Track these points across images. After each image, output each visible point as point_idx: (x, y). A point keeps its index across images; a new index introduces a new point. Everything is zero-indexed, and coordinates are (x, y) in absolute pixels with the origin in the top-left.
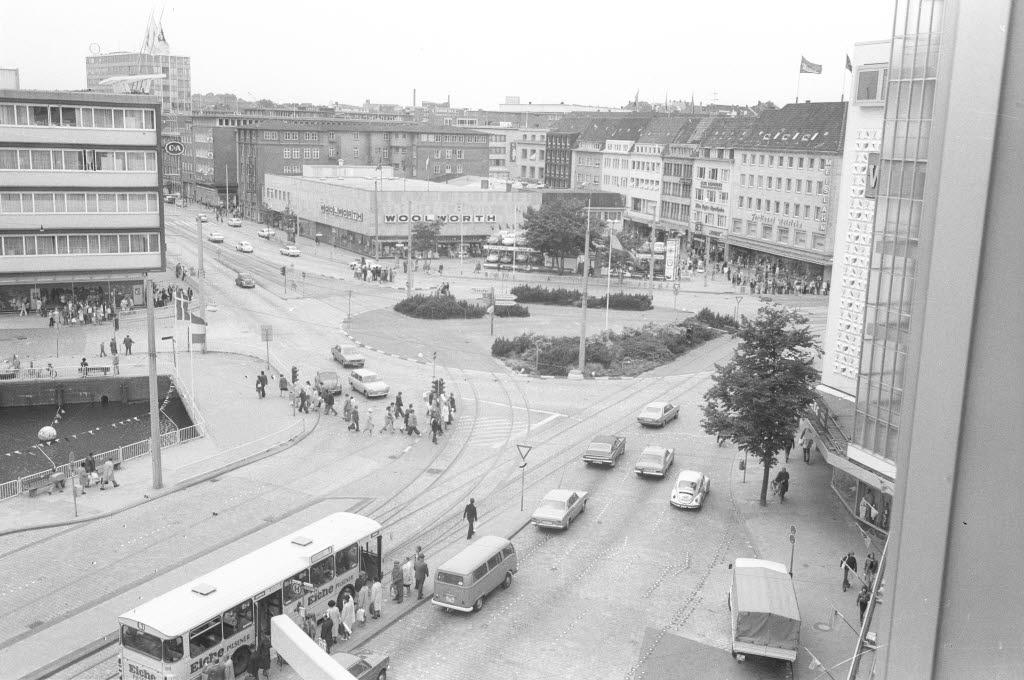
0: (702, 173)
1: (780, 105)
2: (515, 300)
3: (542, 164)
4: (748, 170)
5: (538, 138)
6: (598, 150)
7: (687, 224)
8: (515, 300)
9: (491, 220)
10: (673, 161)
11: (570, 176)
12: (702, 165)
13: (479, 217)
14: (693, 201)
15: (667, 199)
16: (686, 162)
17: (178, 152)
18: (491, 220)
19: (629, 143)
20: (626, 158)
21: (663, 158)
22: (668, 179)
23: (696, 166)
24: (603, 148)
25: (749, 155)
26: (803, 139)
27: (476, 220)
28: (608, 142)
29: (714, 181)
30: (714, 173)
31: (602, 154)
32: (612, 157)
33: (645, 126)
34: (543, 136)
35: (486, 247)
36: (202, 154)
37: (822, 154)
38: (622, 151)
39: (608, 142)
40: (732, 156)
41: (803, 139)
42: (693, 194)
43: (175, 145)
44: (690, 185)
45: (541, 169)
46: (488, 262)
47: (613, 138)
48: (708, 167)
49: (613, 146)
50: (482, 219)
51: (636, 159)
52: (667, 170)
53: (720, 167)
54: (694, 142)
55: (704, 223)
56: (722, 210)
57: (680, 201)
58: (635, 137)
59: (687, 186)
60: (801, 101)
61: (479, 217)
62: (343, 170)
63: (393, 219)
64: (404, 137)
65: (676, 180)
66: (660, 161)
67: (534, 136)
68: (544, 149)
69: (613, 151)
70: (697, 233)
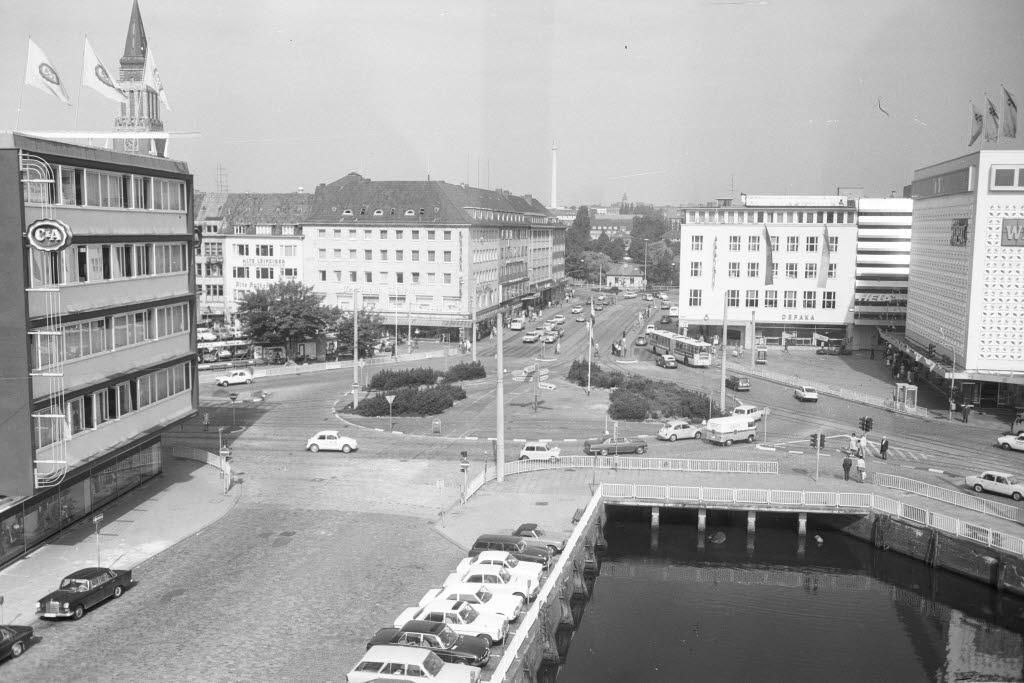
40: (299, 229)
42: (228, 270)
48: (252, 244)
53: (276, 244)
54: (209, 219)
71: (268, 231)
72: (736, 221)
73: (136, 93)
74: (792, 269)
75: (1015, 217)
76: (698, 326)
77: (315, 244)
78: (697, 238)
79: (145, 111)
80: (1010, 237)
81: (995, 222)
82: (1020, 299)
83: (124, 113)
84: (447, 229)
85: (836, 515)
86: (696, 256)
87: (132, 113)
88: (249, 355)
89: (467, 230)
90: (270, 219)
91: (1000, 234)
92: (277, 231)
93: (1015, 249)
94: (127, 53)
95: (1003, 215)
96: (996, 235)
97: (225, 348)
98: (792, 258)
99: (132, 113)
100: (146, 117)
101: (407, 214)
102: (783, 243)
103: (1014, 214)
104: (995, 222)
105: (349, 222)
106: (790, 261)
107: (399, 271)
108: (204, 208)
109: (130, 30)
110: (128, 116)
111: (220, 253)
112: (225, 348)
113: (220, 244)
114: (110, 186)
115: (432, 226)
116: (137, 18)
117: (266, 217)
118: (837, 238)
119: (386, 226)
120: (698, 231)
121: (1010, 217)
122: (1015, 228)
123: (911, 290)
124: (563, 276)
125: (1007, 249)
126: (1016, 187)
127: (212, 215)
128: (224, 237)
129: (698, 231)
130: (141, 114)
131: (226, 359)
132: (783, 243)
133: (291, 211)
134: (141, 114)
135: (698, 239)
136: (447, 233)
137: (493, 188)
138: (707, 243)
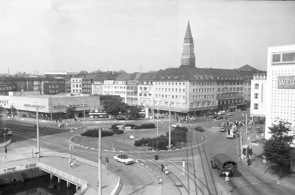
0: (141, 88)
1: (164, 69)
2: (131, 128)
3: (81, 89)
4: (158, 87)
5: (78, 81)
6: (101, 84)
7: (137, 103)
8: (131, 128)
9: (86, 106)
10: (130, 86)
11: (91, 91)
12: (141, 86)
13: (82, 105)
14: (138, 97)
15: (129, 96)
16: (136, 86)
17: (5, 87)
18: (86, 106)
19: (113, 81)
20: (112, 85)
21: (126, 85)
22: (128, 91)
23: (139, 87)
24: (103, 83)
25: (158, 83)
26: (162, 78)
27: (81, 106)
28: (105, 81)
29: (146, 90)
30: (145, 88)
31: (103, 85)
32: (107, 86)
33: (117, 76)
34: (80, 80)
35: (90, 114)
36: (88, 86)
37: (184, 81)
38: (110, 84)
39: (105, 81)
40: (152, 83)
41: (162, 78)
42: (138, 94)
43: (4, 84)
44: (137, 92)
45: (80, 90)
46: (90, 118)
47: (106, 80)
48: (143, 86)
49: (106, 82)
50: (83, 105)
51: (116, 86)
52: (128, 88)
53: (147, 86)
54: (136, 80)
55: (143, 102)
56: (150, 99)
57: (134, 97)
58: (115, 80)
59: (136, 93)
60: (170, 68)
61: (82, 105)
62: (23, 93)
63: (56, 107)
64: (38, 82)
65: (133, 91)
66: (125, 86)
67: (77, 80)
68: (81, 84)
69: (107, 83)
70: (141, 105)
72: (261, 78)
73: (185, 47)
75: (283, 75)
77: (155, 87)
78: (257, 84)
79: (189, 51)
81: (275, 78)
82: (293, 113)
83: (184, 52)
84: (180, 82)
85: (65, 181)
86: (257, 91)
87: (186, 52)
88: (108, 117)
89: (188, 82)
91: (277, 83)
92: (147, 84)
93: (290, 90)
94: (186, 36)
96: (276, 84)
97: (101, 115)
99: (186, 52)
100: (189, 52)
103: (283, 74)
104: (275, 78)
105: (162, 80)
109: (187, 30)
111: (137, 89)
112: (101, 115)
113: (137, 87)
115: (180, 81)
116: (189, 27)
118: (258, 84)
119: (170, 81)
120: (257, 82)
121: (281, 75)
124: (70, 96)
125: (281, 90)
128: (138, 85)
129: (257, 82)
130: (188, 52)
131: (101, 118)
134: (188, 52)
135: (257, 85)
136: (180, 83)
137: (205, 68)
138: (260, 86)
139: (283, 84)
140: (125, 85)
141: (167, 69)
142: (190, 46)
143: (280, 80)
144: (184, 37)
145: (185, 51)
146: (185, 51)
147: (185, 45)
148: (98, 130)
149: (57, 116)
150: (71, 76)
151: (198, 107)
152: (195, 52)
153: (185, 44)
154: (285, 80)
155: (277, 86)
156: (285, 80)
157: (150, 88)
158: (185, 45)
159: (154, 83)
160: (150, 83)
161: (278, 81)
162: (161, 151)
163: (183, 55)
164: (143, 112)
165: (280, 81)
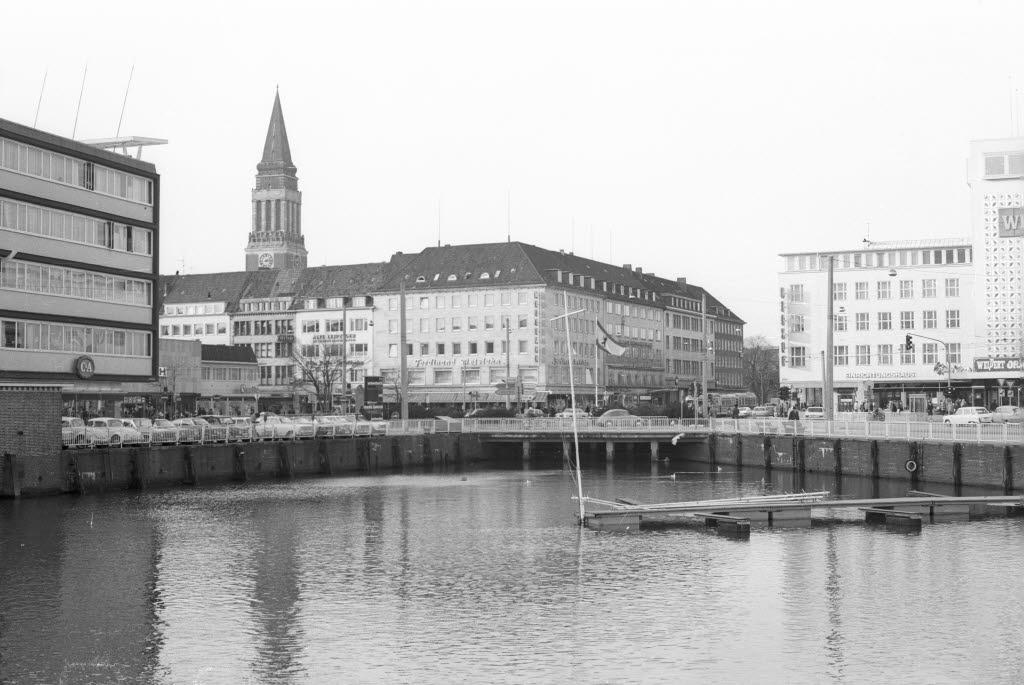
21: (232, 316)
40: (369, 301)
48: (322, 317)
60: (442, 245)
71: (340, 302)
74: (862, 321)
76: (869, 441)
80: (1007, 226)
87: (268, 227)
90: (341, 292)
91: (997, 226)
95: (998, 206)
98: (861, 306)
99: (268, 227)
101: (418, 281)
102: (851, 291)
106: (928, 309)
107: (473, 341)
108: (278, 285)
110: (263, 230)
114: (837, 304)
117: (339, 290)
122: (1011, 218)
123: (581, 341)
125: (1007, 240)
126: (1006, 174)
127: (285, 291)
130: (278, 227)
132: (851, 291)
133: (365, 282)
134: (278, 227)
139: (1014, 227)
140: (228, 318)
141: (428, 251)
142: (288, 201)
143: (1005, 217)
144: (258, 158)
145: (263, 223)
146: (263, 223)
147: (264, 195)
148: (521, 444)
149: (583, 644)
150: (838, 253)
151: (160, 332)
152: (304, 231)
153: (264, 192)
154: (1017, 217)
155: (997, 231)
156: (1017, 217)
157: (359, 325)
158: (264, 195)
159: (380, 300)
160: (360, 301)
161: (1001, 218)
162: (374, 386)
163: (253, 238)
164: (1012, 370)
165: (1005, 221)
